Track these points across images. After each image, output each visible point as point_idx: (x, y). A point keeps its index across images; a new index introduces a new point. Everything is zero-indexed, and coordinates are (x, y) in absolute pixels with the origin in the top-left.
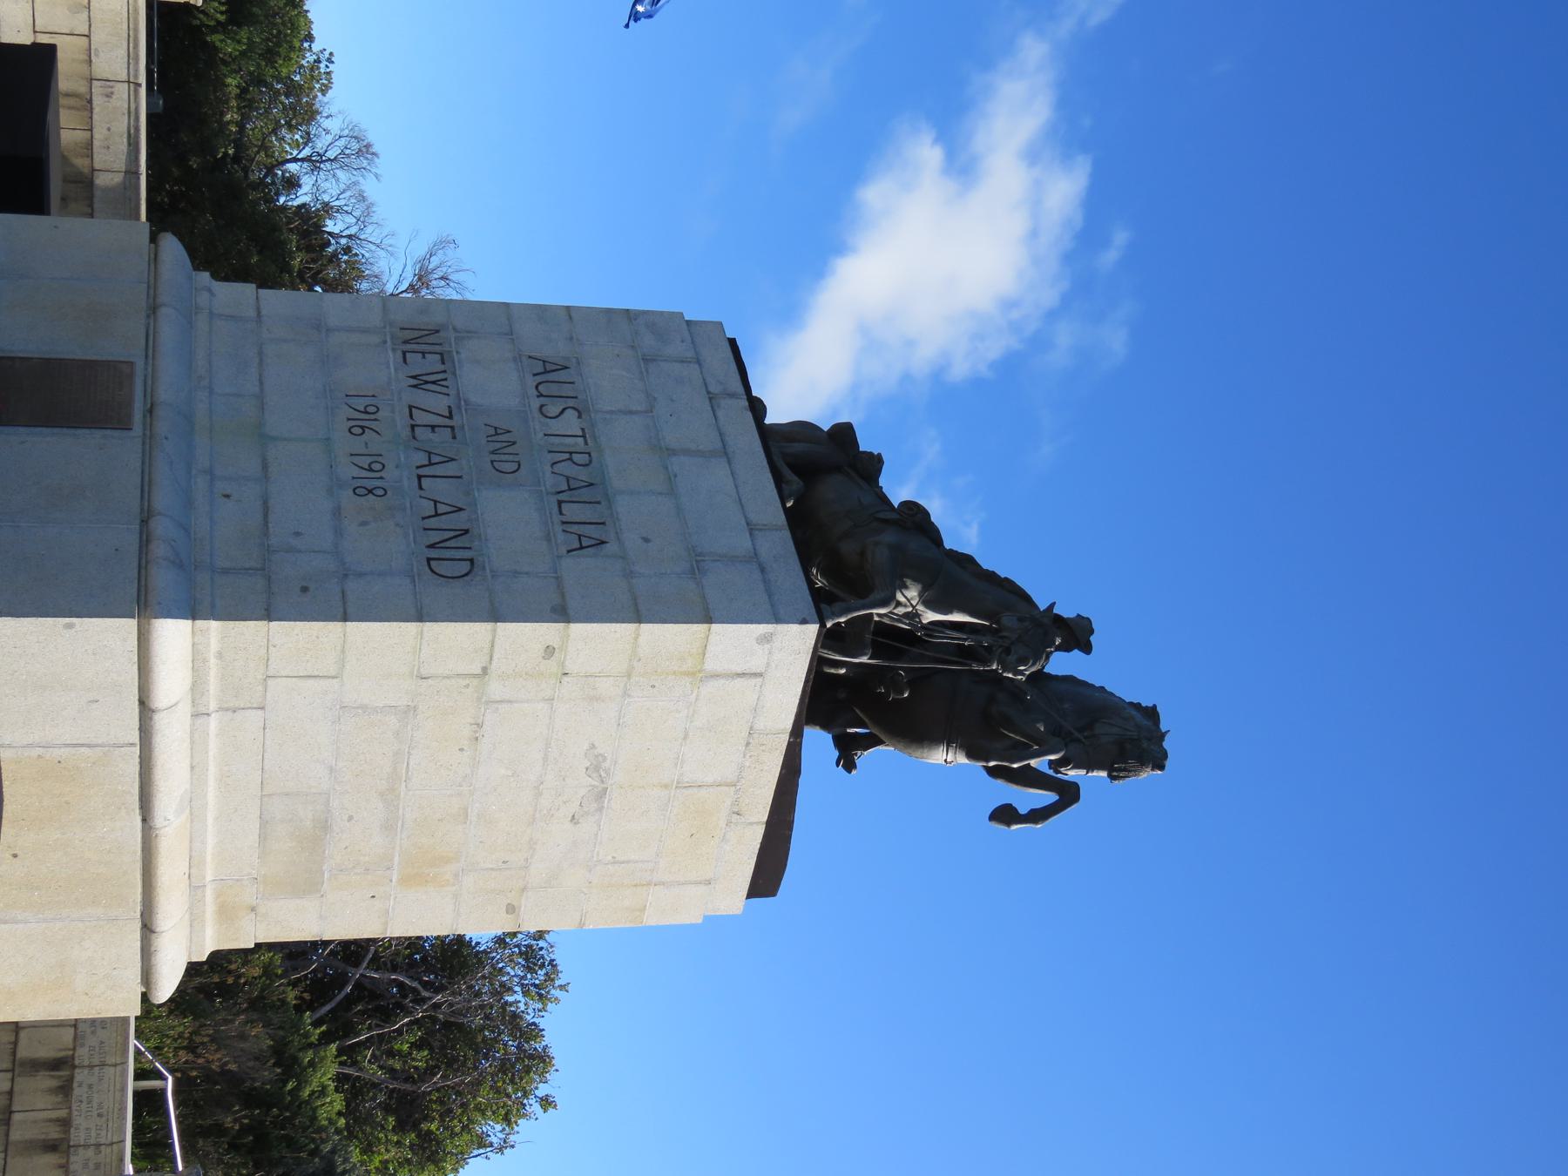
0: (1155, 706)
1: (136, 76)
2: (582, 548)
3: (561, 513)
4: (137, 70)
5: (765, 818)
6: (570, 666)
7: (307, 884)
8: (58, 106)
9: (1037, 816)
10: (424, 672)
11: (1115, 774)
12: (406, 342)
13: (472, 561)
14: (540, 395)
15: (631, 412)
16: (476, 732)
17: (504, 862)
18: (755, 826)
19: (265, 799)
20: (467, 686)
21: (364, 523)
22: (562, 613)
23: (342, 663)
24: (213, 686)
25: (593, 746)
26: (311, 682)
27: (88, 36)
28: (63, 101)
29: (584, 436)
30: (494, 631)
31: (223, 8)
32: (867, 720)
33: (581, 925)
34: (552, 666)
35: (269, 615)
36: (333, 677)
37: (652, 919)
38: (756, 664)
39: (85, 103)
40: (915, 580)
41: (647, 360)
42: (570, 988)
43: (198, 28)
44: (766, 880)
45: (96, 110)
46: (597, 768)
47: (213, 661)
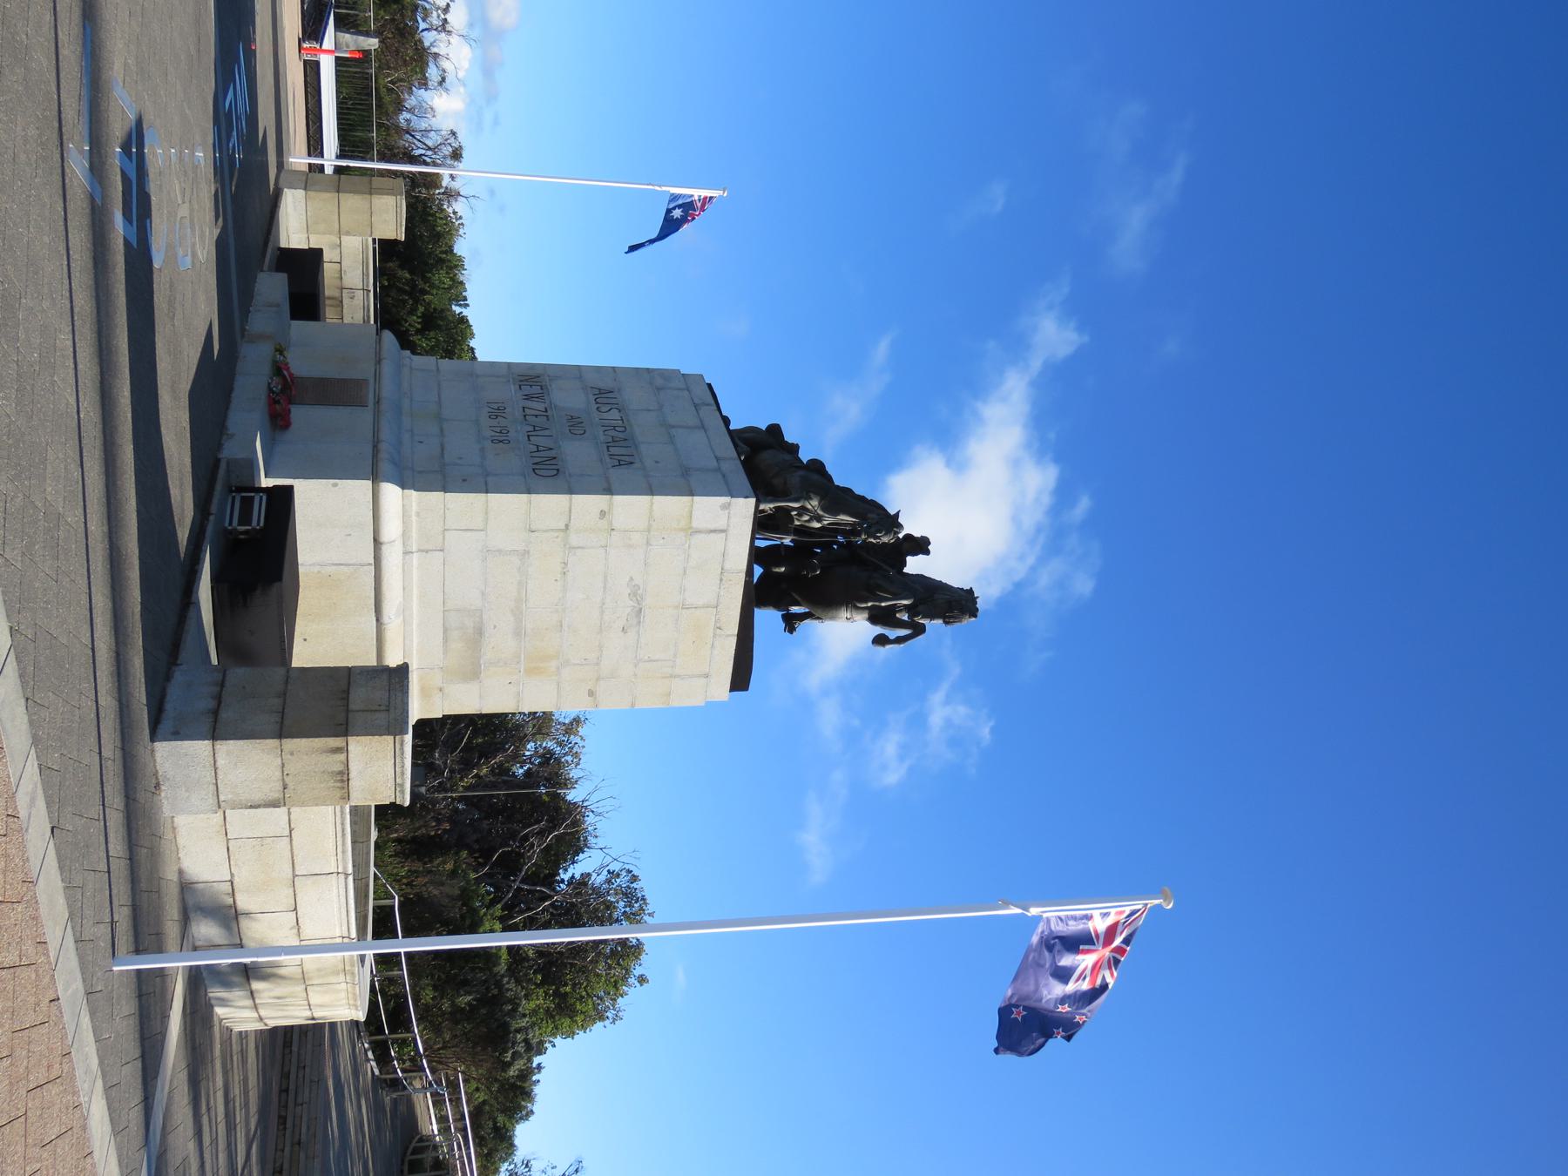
0: (971, 588)
1: (368, 286)
2: (620, 465)
3: (608, 451)
4: (368, 282)
5: (736, 632)
6: (616, 525)
7: (473, 672)
8: (325, 305)
9: (899, 640)
10: (533, 528)
11: (947, 620)
12: (521, 381)
13: (558, 470)
14: (597, 403)
15: (649, 410)
16: (564, 568)
17: (585, 659)
18: (730, 638)
19: (446, 613)
20: (557, 537)
21: (497, 454)
22: (609, 490)
23: (486, 520)
24: (414, 535)
25: (631, 579)
26: (469, 534)
27: (340, 263)
28: (327, 302)
29: (622, 420)
30: (571, 500)
31: (419, 320)
32: (799, 599)
33: (633, 705)
34: (604, 524)
35: (445, 489)
36: (481, 530)
37: (676, 702)
38: (721, 524)
39: (338, 303)
40: (816, 494)
41: (659, 389)
42: (655, 915)
43: (406, 859)
44: (741, 678)
45: (345, 307)
46: (635, 594)
47: (414, 518)
